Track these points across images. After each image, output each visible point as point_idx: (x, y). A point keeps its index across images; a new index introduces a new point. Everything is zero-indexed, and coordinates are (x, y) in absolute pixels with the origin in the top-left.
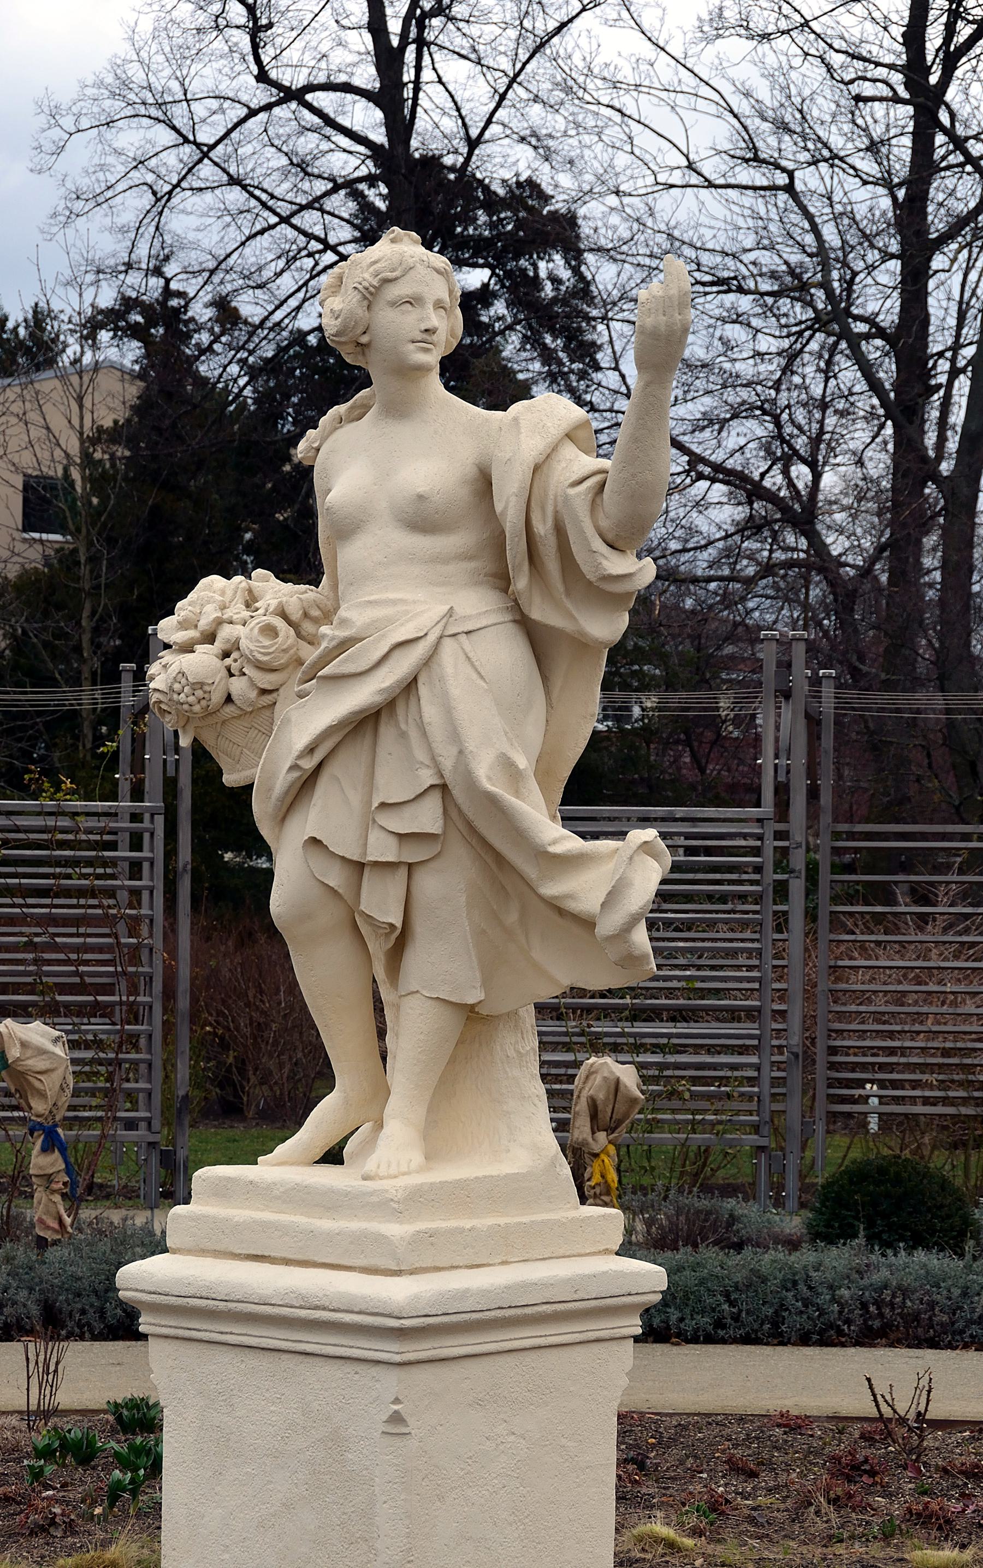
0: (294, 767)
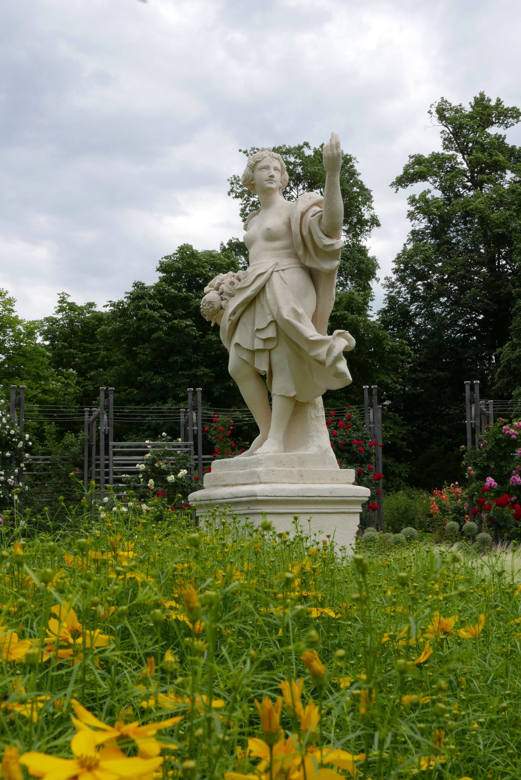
0: (229, 320)
